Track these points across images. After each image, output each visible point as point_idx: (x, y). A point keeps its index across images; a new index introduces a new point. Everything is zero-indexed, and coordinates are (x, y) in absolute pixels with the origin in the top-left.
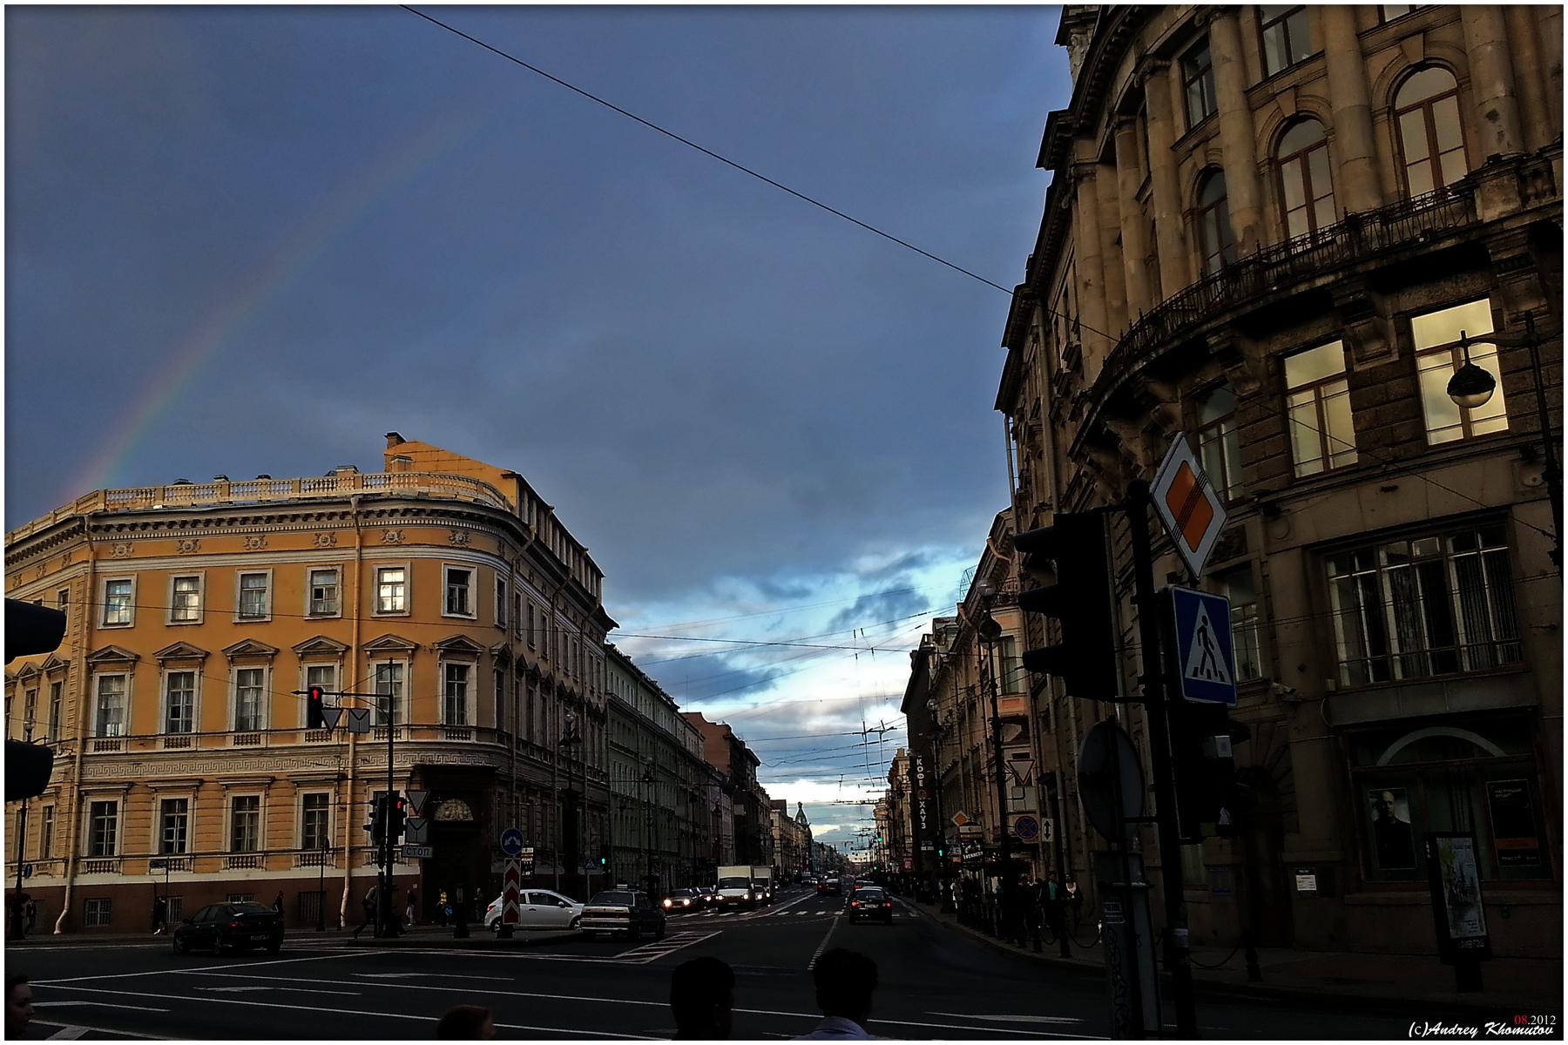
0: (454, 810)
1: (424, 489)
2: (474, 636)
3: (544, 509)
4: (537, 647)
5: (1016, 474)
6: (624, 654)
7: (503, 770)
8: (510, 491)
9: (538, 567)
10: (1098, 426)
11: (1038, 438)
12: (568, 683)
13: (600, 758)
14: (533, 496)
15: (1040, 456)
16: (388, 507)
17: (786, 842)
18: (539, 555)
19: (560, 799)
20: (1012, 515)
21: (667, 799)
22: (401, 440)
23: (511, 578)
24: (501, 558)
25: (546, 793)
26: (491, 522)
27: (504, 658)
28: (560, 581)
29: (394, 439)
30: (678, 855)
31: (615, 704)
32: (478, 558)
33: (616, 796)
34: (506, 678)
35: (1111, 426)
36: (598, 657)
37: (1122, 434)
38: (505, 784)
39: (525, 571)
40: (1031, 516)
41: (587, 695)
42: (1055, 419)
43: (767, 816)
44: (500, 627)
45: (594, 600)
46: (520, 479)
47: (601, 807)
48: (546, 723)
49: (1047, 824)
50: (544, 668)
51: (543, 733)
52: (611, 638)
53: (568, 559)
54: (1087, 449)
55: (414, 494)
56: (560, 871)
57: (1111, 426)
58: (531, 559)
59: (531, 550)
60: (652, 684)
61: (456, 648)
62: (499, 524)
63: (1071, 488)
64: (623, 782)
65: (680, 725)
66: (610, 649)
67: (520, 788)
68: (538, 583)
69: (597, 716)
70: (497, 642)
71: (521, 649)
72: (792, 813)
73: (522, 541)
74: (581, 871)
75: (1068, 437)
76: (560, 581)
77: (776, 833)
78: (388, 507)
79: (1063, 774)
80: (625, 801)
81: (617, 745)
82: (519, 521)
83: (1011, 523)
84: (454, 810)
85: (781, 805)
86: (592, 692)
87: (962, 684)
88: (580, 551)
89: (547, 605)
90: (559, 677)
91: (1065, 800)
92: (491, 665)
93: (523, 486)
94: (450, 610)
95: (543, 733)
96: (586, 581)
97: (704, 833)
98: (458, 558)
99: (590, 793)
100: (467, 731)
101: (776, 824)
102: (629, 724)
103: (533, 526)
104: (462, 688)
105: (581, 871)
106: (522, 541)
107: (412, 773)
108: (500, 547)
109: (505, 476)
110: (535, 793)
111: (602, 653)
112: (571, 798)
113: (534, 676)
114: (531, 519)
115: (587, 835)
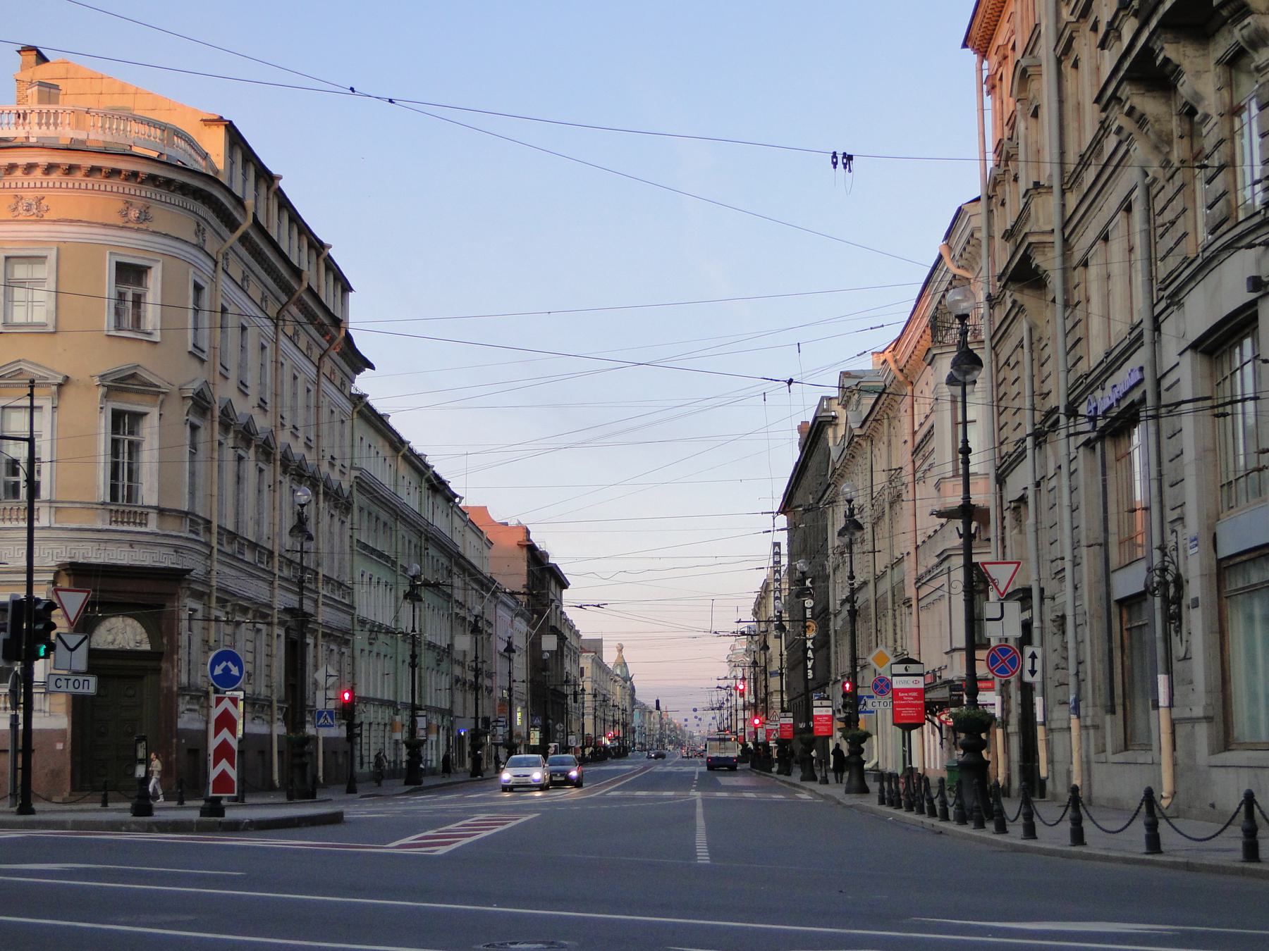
0: (122, 633)
1: (82, 135)
2: (155, 368)
3: (265, 177)
4: (253, 391)
5: (990, 147)
6: (380, 411)
7: (199, 570)
8: (215, 144)
9: (257, 268)
10: (1148, 51)
11: (1033, 86)
12: (298, 449)
13: (341, 561)
14: (249, 157)
15: (1035, 114)
16: (22, 159)
17: (602, 700)
18: (259, 247)
19: (282, 623)
20: (981, 207)
21: (435, 630)
22: (42, 59)
23: (213, 280)
24: (201, 248)
25: (261, 613)
26: (184, 189)
27: (201, 403)
28: (288, 290)
29: (32, 57)
30: (450, 712)
31: (365, 485)
32: (169, 247)
33: (363, 622)
34: (202, 435)
35: (1170, 51)
36: (343, 412)
37: (1186, 65)
38: (199, 596)
39: (236, 270)
40: (1014, 204)
41: (325, 468)
42: (1065, 49)
43: (576, 662)
44: (196, 354)
45: (337, 322)
46: (231, 129)
47: (340, 637)
48: (262, 508)
49: (1033, 656)
50: (262, 423)
51: (258, 523)
52: (362, 383)
53: (299, 256)
54: (1126, 90)
55: (64, 142)
56: (279, 729)
57: (1170, 51)
58: (243, 252)
59: (244, 239)
60: (419, 457)
61: (120, 384)
62: (197, 194)
63: (1084, 162)
64: (376, 602)
65: (458, 522)
66: (359, 401)
67: (222, 602)
68: (255, 291)
69: (339, 501)
70: (192, 377)
71: (225, 392)
72: (609, 658)
73: (232, 225)
74: (310, 730)
75: (1084, 86)
76: (288, 290)
77: (588, 686)
78: (22, 159)
79: (1042, 590)
80: (376, 630)
81: (365, 547)
82: (228, 191)
83: (979, 221)
84: (122, 633)
85: (595, 647)
86: (332, 465)
87: (881, 464)
88: (317, 247)
89: (269, 329)
90: (284, 438)
91: (1042, 629)
92: (179, 412)
93: (235, 138)
94: (118, 327)
95: (258, 523)
96: (327, 293)
97: (487, 682)
98: (133, 246)
99: (325, 615)
100: (140, 516)
101: (587, 673)
102: (384, 516)
103: (249, 202)
104: (134, 447)
105: (310, 730)
106: (232, 225)
107: (57, 574)
108: (199, 231)
109: (207, 122)
110: (244, 610)
111: (348, 407)
112: (299, 622)
113: (246, 435)
114: (244, 187)
115: (320, 676)
